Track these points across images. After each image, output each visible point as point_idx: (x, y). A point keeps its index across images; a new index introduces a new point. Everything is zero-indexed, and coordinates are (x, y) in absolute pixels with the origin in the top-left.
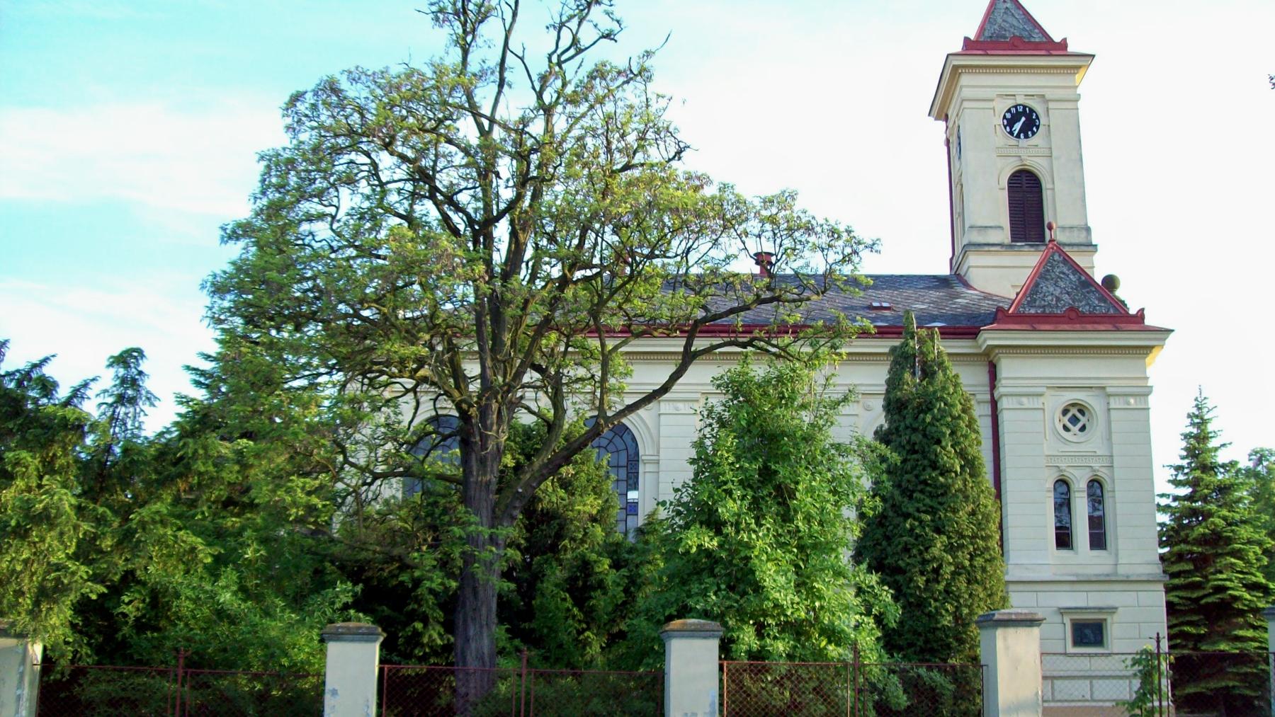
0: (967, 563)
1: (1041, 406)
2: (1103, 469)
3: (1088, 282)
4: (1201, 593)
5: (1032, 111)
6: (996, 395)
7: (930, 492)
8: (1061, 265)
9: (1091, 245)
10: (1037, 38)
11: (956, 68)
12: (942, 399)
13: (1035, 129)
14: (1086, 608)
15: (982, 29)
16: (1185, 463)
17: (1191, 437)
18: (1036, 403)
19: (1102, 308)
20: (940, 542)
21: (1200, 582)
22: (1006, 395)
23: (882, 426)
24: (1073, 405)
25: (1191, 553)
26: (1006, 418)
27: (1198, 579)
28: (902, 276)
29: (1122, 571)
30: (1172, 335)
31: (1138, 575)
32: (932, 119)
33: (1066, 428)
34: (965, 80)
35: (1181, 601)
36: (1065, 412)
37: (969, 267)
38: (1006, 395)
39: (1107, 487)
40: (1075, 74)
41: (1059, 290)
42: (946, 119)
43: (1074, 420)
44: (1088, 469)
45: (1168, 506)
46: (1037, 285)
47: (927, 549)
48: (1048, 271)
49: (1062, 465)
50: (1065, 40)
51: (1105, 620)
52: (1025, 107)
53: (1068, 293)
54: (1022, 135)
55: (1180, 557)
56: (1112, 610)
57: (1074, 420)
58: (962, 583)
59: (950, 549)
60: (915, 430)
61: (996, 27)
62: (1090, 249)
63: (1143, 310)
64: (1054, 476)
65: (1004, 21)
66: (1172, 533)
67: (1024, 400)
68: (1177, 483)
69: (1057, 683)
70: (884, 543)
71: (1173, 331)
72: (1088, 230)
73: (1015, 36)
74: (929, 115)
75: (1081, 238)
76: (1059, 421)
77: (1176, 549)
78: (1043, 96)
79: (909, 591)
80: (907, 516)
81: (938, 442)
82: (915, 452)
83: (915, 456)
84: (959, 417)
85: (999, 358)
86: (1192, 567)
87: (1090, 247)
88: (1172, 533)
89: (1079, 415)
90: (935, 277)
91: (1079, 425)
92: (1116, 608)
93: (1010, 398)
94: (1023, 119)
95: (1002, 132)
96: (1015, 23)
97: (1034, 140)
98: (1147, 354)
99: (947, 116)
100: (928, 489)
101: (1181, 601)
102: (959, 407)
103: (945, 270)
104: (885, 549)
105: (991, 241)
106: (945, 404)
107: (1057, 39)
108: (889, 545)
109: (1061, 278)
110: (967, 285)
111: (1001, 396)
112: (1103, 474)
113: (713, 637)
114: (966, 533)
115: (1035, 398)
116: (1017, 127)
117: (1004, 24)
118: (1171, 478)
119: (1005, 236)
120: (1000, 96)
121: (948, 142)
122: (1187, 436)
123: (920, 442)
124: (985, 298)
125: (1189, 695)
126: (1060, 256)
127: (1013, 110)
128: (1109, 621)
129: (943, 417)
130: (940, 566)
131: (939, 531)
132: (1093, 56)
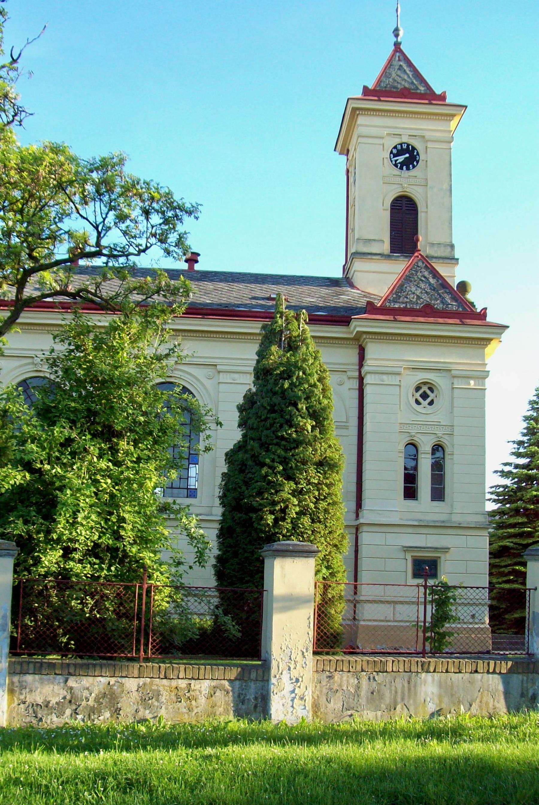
0: (312, 506)
1: (398, 383)
2: (445, 436)
3: (445, 285)
4: (530, 541)
5: (414, 148)
6: (363, 374)
7: (285, 446)
8: (423, 270)
9: (453, 259)
10: (422, 89)
11: (354, 110)
12: (300, 368)
13: (415, 163)
14: (424, 548)
15: (379, 81)
16: (525, 439)
17: (532, 419)
18: (395, 380)
19: (454, 306)
20: (288, 486)
21: (530, 531)
22: (369, 373)
23: (250, 390)
24: (425, 383)
25: (526, 509)
26: (368, 390)
27: (529, 529)
28: (302, 277)
29: (456, 519)
30: (507, 331)
31: (468, 523)
32: (337, 153)
33: (418, 402)
34: (361, 120)
35: (515, 546)
36: (418, 389)
37: (354, 272)
38: (369, 373)
39: (447, 451)
40: (450, 120)
41: (420, 290)
42: (347, 155)
43: (425, 396)
44: (433, 436)
45: (510, 472)
46: (402, 286)
47: (277, 492)
48: (412, 274)
49: (413, 432)
50: (444, 93)
51: (440, 557)
52: (408, 145)
53: (427, 293)
54: (404, 168)
55: (517, 512)
56: (446, 550)
57: (425, 396)
58: (306, 520)
59: (298, 493)
60: (275, 393)
61: (391, 80)
62: (453, 262)
63: (485, 309)
64: (406, 440)
65: (398, 75)
66: (512, 493)
67: (385, 377)
68: (519, 455)
69: (399, 607)
70: (244, 488)
71: (508, 327)
72: (452, 246)
73: (405, 88)
74: (335, 150)
75: (446, 252)
76: (410, 396)
77: (514, 505)
78: (423, 137)
79: (259, 527)
80: (263, 465)
81: (295, 405)
82: (274, 412)
83: (273, 415)
84: (315, 386)
85: (367, 342)
86: (525, 520)
87: (452, 260)
88: (512, 493)
89: (428, 392)
90: (328, 279)
91: (429, 400)
92: (449, 549)
93: (373, 375)
94: (407, 155)
95: (389, 165)
96: (406, 77)
97: (413, 172)
98: (487, 345)
99: (348, 151)
100: (283, 443)
101: (515, 546)
102: (316, 377)
103: (338, 274)
104: (243, 492)
105: (374, 251)
106: (304, 373)
107: (438, 92)
108: (247, 489)
109: (422, 281)
110: (352, 286)
111: (367, 373)
112: (446, 441)
113: (8, 555)
114: (312, 480)
115: (393, 376)
116: (401, 159)
117: (397, 78)
118: (514, 451)
119: (386, 248)
120: (388, 134)
121: (348, 171)
122: (527, 418)
123: (279, 404)
124: (365, 296)
125: (515, 618)
126: (423, 263)
127: (399, 147)
128: (443, 559)
129: (301, 384)
130: (287, 507)
131: (289, 478)
132: (466, 107)
